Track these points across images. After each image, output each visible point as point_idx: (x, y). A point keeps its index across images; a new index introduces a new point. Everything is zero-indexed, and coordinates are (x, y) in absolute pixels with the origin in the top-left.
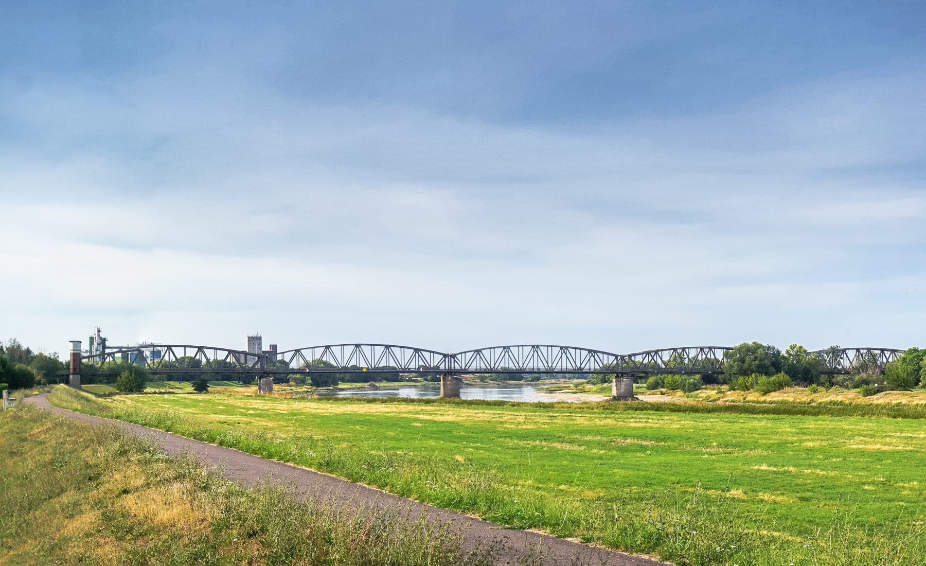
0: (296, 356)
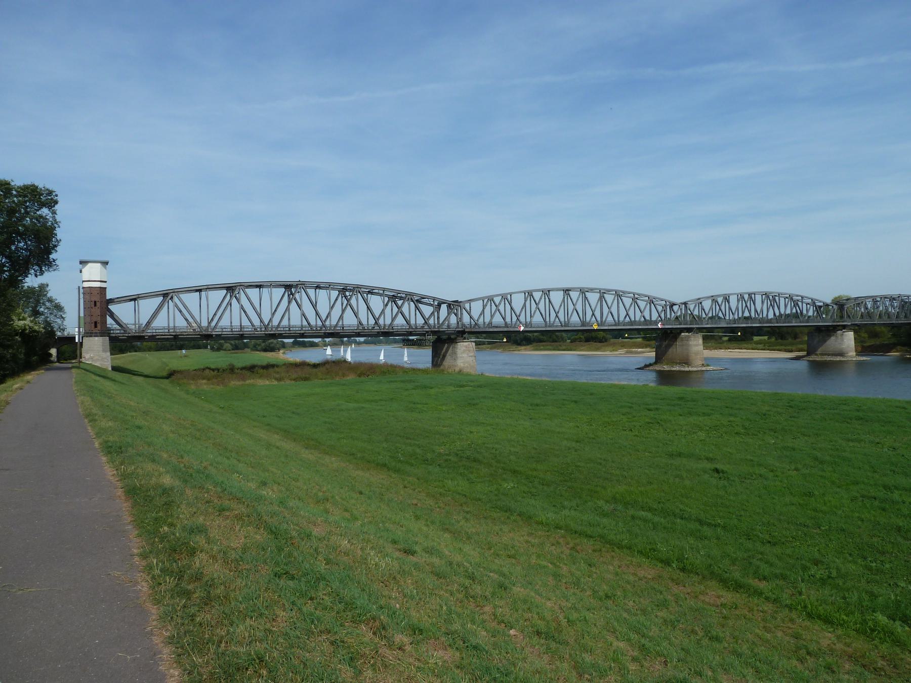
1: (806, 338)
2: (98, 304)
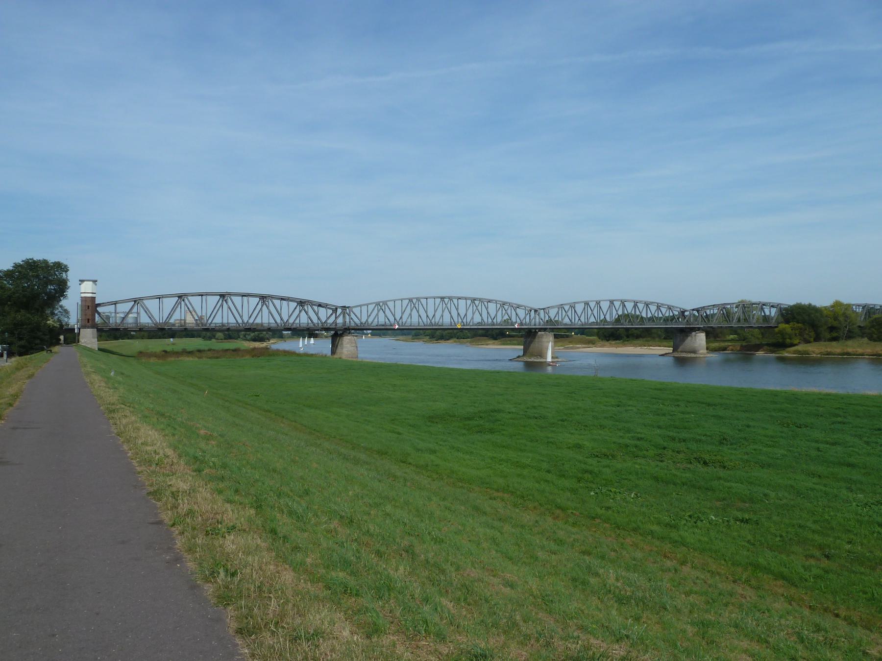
0: (179, 309)
2: (90, 308)
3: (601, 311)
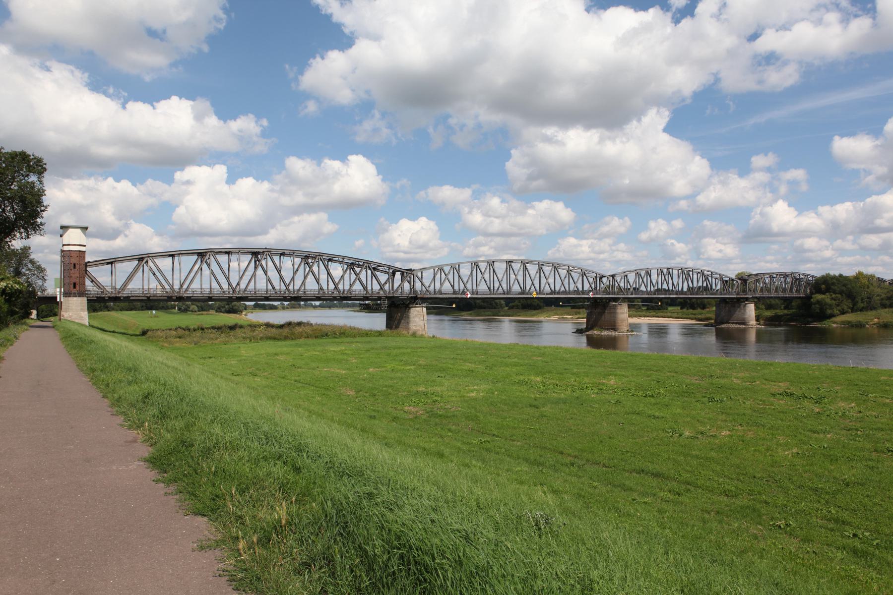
1: (714, 308)
2: (77, 266)
3: (495, 276)
